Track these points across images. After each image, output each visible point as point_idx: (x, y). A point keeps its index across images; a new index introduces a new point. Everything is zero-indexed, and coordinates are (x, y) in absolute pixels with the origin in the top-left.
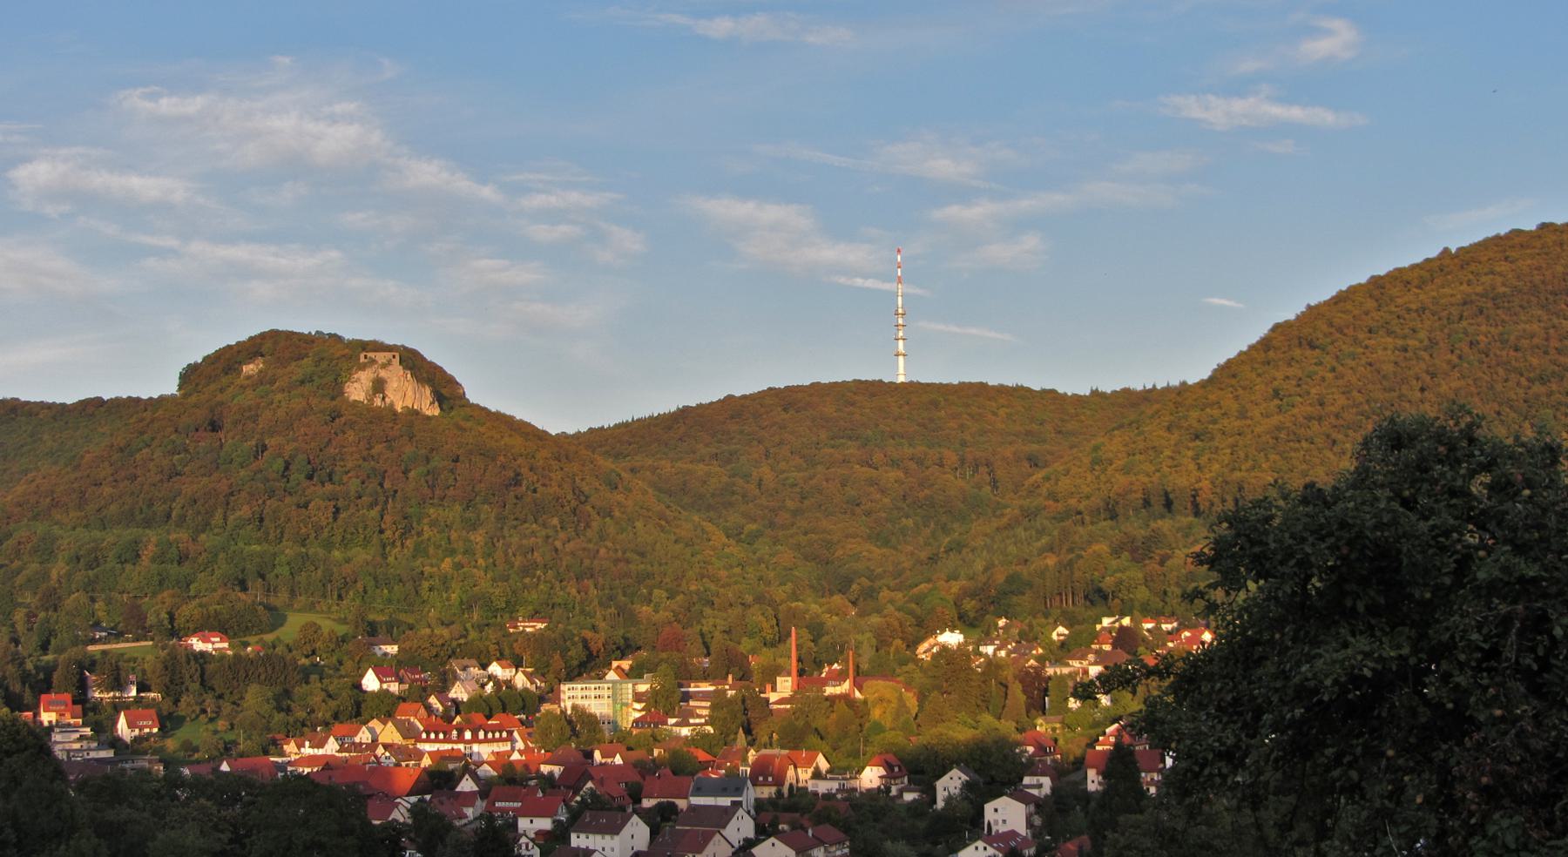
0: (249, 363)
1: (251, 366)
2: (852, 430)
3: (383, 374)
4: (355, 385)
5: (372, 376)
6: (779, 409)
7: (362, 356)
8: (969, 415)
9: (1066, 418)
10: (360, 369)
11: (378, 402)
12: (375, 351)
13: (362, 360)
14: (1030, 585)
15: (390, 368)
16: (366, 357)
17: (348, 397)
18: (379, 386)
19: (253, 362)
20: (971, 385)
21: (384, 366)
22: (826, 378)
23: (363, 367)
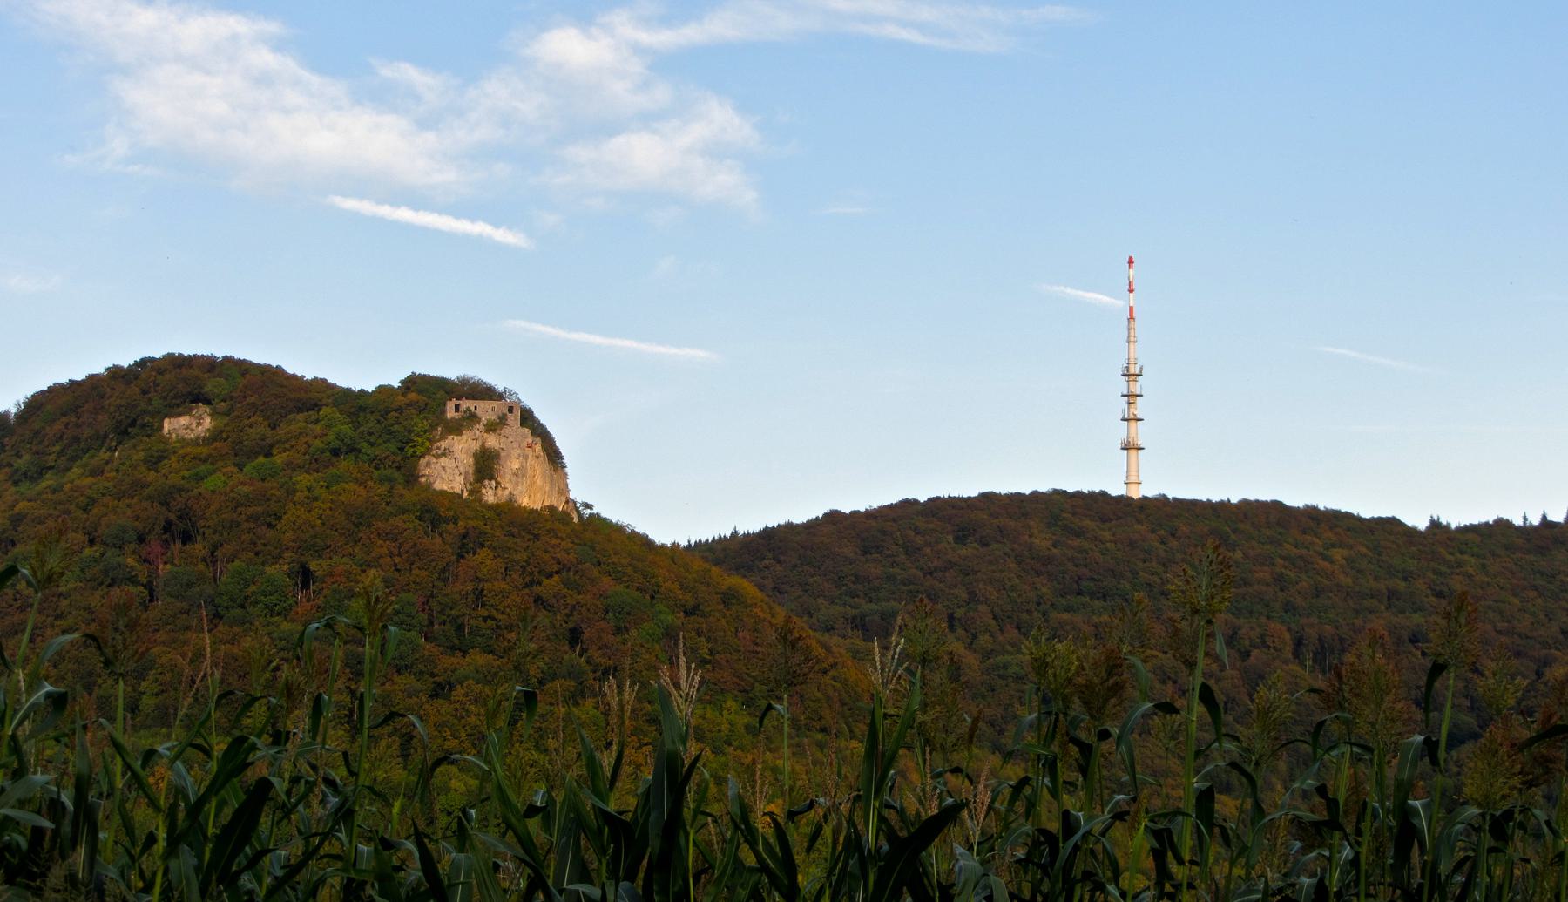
0: (180, 415)
1: (184, 420)
2: (1092, 579)
3: (492, 441)
4: (443, 461)
5: (476, 446)
6: (950, 538)
7: (450, 405)
8: (1284, 558)
9: (1443, 569)
10: (450, 433)
11: (490, 497)
12: (474, 398)
13: (450, 413)
14: (411, 804)
15: (506, 430)
16: (457, 407)
17: (429, 485)
18: (486, 465)
19: (189, 412)
20: (1259, 505)
21: (491, 428)
22: (1005, 485)
23: (456, 428)
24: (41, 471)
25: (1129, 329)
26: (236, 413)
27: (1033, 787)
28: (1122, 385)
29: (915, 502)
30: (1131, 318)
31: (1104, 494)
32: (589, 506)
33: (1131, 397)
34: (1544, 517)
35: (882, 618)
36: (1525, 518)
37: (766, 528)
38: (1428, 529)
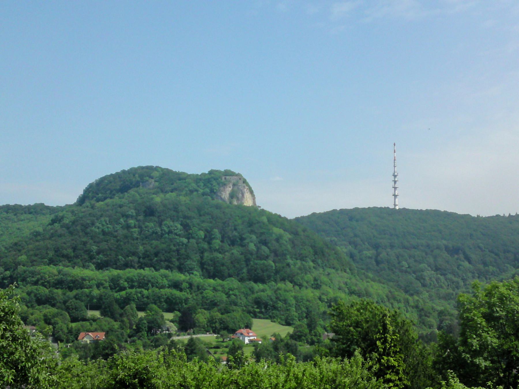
24: (105, 198)
25: (394, 163)
26: (410, 298)
27: (410, 306)
28: (393, 178)
29: (336, 210)
30: (395, 160)
31: (388, 208)
32: (260, 207)
33: (395, 182)
34: (510, 214)
35: (387, 254)
36: (504, 215)
37: (427, 209)
38: (508, 216)
